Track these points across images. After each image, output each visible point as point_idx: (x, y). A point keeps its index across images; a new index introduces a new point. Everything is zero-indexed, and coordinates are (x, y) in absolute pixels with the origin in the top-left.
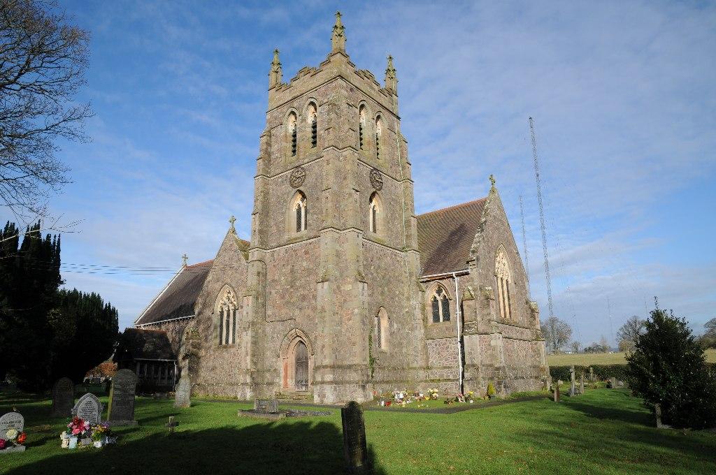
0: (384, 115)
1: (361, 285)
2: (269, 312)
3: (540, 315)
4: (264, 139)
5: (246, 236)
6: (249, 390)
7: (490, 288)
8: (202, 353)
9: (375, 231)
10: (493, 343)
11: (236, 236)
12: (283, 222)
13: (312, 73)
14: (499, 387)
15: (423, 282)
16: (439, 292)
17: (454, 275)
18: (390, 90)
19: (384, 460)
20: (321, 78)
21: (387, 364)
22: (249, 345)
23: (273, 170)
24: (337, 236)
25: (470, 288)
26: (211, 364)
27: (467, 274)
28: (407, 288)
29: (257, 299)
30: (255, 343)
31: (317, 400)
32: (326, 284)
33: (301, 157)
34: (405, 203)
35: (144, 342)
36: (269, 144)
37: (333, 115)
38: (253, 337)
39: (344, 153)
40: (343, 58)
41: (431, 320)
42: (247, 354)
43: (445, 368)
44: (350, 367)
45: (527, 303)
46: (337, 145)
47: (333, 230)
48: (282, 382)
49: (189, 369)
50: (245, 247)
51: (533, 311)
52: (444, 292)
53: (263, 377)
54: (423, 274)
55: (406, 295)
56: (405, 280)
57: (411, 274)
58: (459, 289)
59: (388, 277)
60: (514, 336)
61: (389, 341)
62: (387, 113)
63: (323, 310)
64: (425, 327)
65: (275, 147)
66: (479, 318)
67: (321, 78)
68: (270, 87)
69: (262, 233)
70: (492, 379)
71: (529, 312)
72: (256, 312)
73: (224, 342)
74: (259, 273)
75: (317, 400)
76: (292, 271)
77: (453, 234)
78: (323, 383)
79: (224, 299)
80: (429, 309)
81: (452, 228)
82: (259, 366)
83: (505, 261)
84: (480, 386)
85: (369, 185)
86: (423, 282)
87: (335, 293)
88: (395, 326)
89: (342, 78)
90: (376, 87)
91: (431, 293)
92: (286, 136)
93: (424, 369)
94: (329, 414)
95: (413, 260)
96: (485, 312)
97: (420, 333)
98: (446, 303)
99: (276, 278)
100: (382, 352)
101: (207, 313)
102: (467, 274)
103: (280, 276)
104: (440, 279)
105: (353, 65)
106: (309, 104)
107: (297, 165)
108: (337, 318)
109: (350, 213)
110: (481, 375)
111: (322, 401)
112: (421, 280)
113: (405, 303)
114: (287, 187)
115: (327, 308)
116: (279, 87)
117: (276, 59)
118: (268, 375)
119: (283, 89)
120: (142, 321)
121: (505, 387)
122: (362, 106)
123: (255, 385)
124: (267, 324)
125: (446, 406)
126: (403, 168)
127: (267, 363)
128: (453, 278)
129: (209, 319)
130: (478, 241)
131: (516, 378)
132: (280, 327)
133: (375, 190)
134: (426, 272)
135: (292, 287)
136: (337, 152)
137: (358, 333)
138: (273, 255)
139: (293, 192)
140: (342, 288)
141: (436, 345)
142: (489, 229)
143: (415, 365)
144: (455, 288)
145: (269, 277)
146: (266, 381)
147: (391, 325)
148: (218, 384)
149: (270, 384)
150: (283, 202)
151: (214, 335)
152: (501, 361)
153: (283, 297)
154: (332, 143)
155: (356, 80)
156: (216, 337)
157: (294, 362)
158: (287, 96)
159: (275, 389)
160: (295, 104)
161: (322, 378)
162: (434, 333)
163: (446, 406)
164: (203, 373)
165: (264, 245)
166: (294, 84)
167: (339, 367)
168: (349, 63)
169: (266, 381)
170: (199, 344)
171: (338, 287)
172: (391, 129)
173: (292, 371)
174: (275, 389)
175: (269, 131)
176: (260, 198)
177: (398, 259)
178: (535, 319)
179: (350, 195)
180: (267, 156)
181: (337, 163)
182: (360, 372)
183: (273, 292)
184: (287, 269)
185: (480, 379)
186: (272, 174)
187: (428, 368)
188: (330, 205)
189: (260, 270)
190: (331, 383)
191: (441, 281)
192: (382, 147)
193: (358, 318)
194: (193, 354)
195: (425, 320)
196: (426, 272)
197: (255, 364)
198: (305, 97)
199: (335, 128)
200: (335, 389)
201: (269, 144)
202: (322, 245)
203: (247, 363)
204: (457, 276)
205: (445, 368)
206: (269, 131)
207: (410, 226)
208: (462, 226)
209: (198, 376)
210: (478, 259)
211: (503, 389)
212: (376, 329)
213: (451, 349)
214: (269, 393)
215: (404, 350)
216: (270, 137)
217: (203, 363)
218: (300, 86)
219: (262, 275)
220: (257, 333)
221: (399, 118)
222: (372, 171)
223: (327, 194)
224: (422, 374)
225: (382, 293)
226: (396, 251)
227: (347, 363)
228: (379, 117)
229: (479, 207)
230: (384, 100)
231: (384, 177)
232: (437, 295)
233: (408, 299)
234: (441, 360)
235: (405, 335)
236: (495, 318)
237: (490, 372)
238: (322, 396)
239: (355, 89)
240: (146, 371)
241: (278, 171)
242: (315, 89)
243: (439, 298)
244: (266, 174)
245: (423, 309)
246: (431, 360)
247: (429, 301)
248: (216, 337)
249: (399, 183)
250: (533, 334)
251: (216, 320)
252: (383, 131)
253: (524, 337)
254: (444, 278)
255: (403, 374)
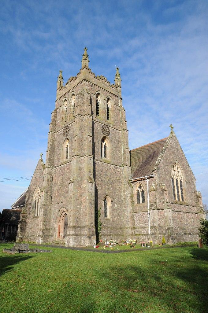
0: (112, 97)
1: (90, 184)
2: (53, 199)
3: (203, 198)
4: (53, 114)
5: (44, 162)
6: (41, 239)
7: (164, 184)
8: (27, 220)
9: (105, 156)
10: (166, 214)
11: (42, 162)
12: (60, 154)
13: (74, 79)
14: (169, 239)
15: (131, 182)
16: (140, 187)
17: (146, 178)
18: (116, 85)
19: (3, 277)
20: (77, 81)
21: (110, 226)
22: (42, 216)
23: (57, 129)
24: (79, 159)
25: (153, 185)
26: (30, 226)
27: (153, 177)
28: (125, 186)
29: (47, 193)
30: (45, 215)
31: (66, 244)
32: (72, 184)
33: (68, 122)
34: (123, 142)
35: (12, 216)
36: (55, 116)
37: (80, 99)
38: (44, 212)
39: (85, 118)
40: (87, 70)
41: (136, 202)
42: (41, 220)
43: (142, 228)
44: (84, 227)
45: (194, 192)
46: (81, 114)
47: (77, 156)
48: (57, 235)
49: (21, 228)
50: (44, 167)
51: (198, 197)
52: (142, 187)
53: (49, 232)
54: (132, 178)
55: (123, 189)
56: (122, 181)
57: (125, 178)
58: (147, 186)
59: (112, 180)
60: (185, 211)
61: (111, 213)
62: (113, 96)
63: (71, 198)
64: (133, 206)
65: (58, 117)
66: (158, 201)
67: (77, 81)
68: (57, 88)
69: (51, 160)
70: (165, 234)
71: (196, 197)
72: (46, 199)
73: (36, 215)
74: (48, 180)
75: (66, 244)
76: (63, 179)
77: (150, 156)
78: (69, 235)
79: (37, 193)
80: (135, 197)
81: (150, 154)
82: (47, 227)
83: (179, 170)
84: (157, 238)
85: (101, 133)
86: (131, 182)
87: (77, 188)
88: (116, 206)
89: (86, 80)
90: (108, 84)
91: (136, 188)
92: (63, 112)
93: (132, 228)
94: (49, 251)
95: (126, 171)
96: (161, 197)
97: (129, 209)
98: (143, 192)
99: (56, 182)
100: (108, 219)
101: (30, 200)
102: (153, 177)
103: (57, 181)
104: (140, 181)
105: (93, 74)
106: (72, 95)
107: (66, 125)
108: (78, 202)
109: (86, 148)
110: (158, 232)
111: (68, 245)
112: (132, 181)
113: (123, 194)
114: (62, 137)
115: (72, 196)
116: (61, 88)
117: (60, 75)
118: (51, 231)
119: (62, 89)
120: (15, 206)
121: (172, 239)
122: (99, 94)
123: (45, 236)
124: (52, 205)
125: (131, 248)
126: (123, 123)
127: (51, 225)
128: (146, 180)
129: (31, 203)
130: (159, 160)
131: (185, 234)
132: (57, 206)
133: (105, 136)
134: (134, 177)
135: (62, 186)
136: (81, 117)
137: (88, 209)
138: (55, 171)
139: (64, 139)
140: (82, 186)
141: (138, 215)
142: (167, 154)
143: (127, 226)
144: (147, 185)
145: (53, 182)
146: (50, 234)
147: (113, 205)
148: (32, 236)
149: (52, 236)
150: (61, 145)
151: (32, 211)
152: (171, 224)
153: (58, 192)
154: (79, 113)
155: (95, 81)
156: (33, 213)
157: (63, 224)
158: (64, 92)
159: (54, 239)
160: (67, 96)
161: (69, 233)
162: (137, 209)
163: (131, 248)
164: (28, 231)
165: (51, 166)
166: (66, 86)
167: (79, 227)
168: (91, 73)
169: (50, 234)
170: (27, 216)
171: (80, 186)
172: (116, 104)
173: (62, 229)
174: (54, 239)
175: (56, 110)
176: (50, 143)
177: (119, 170)
178: (199, 201)
179: (87, 138)
180: (55, 122)
181: (81, 123)
182: (88, 229)
183: (55, 189)
184: (60, 178)
185: (157, 234)
186: (56, 131)
187: (134, 228)
188: (76, 144)
189: (49, 178)
190: (73, 235)
191: (140, 182)
192: (110, 114)
193: (88, 201)
194: (23, 221)
195: (133, 202)
196: (134, 177)
197: (45, 226)
198: (70, 92)
199: (81, 106)
200: (75, 239)
201: (55, 116)
202: (72, 165)
203: (41, 225)
204: (148, 178)
205: (142, 228)
206: (56, 110)
207: (125, 153)
208: (155, 152)
209: (25, 232)
210: (158, 169)
211: (171, 240)
212: (104, 207)
213: (145, 217)
214: (51, 240)
215: (122, 218)
216: (56, 113)
217: (28, 226)
218: (69, 87)
219: (50, 181)
220: (46, 210)
221: (121, 99)
222: (103, 126)
223: (75, 139)
224: (130, 231)
225: (108, 189)
226: (118, 167)
227: (83, 225)
228: (109, 99)
229: (163, 142)
230: (113, 90)
231: (111, 129)
232: (139, 189)
233: (124, 191)
234: (141, 223)
235: (122, 210)
236: (168, 200)
237: (164, 230)
238: (69, 242)
239: (94, 85)
240: (11, 230)
241: (59, 129)
242: (74, 87)
243: (140, 190)
244: (53, 131)
245: (132, 196)
246: (136, 224)
247: (135, 192)
248: (33, 213)
249: (121, 131)
250: (198, 210)
251: (33, 204)
252: (111, 106)
253: (192, 211)
254: (141, 180)
255: (120, 231)
